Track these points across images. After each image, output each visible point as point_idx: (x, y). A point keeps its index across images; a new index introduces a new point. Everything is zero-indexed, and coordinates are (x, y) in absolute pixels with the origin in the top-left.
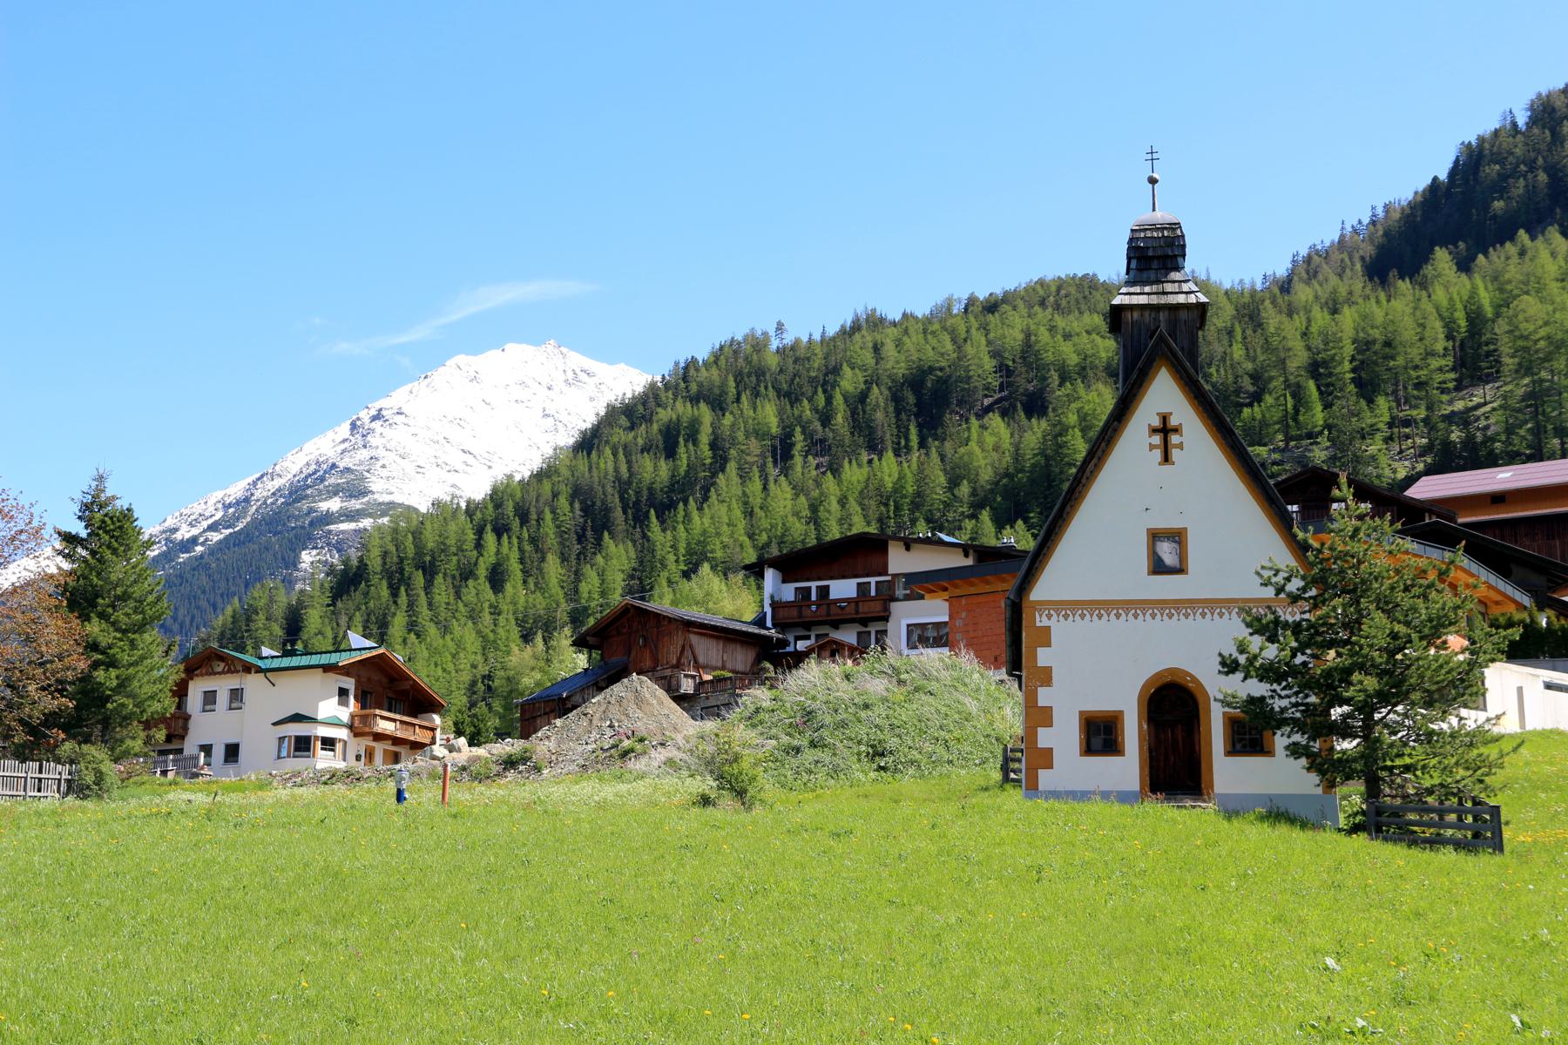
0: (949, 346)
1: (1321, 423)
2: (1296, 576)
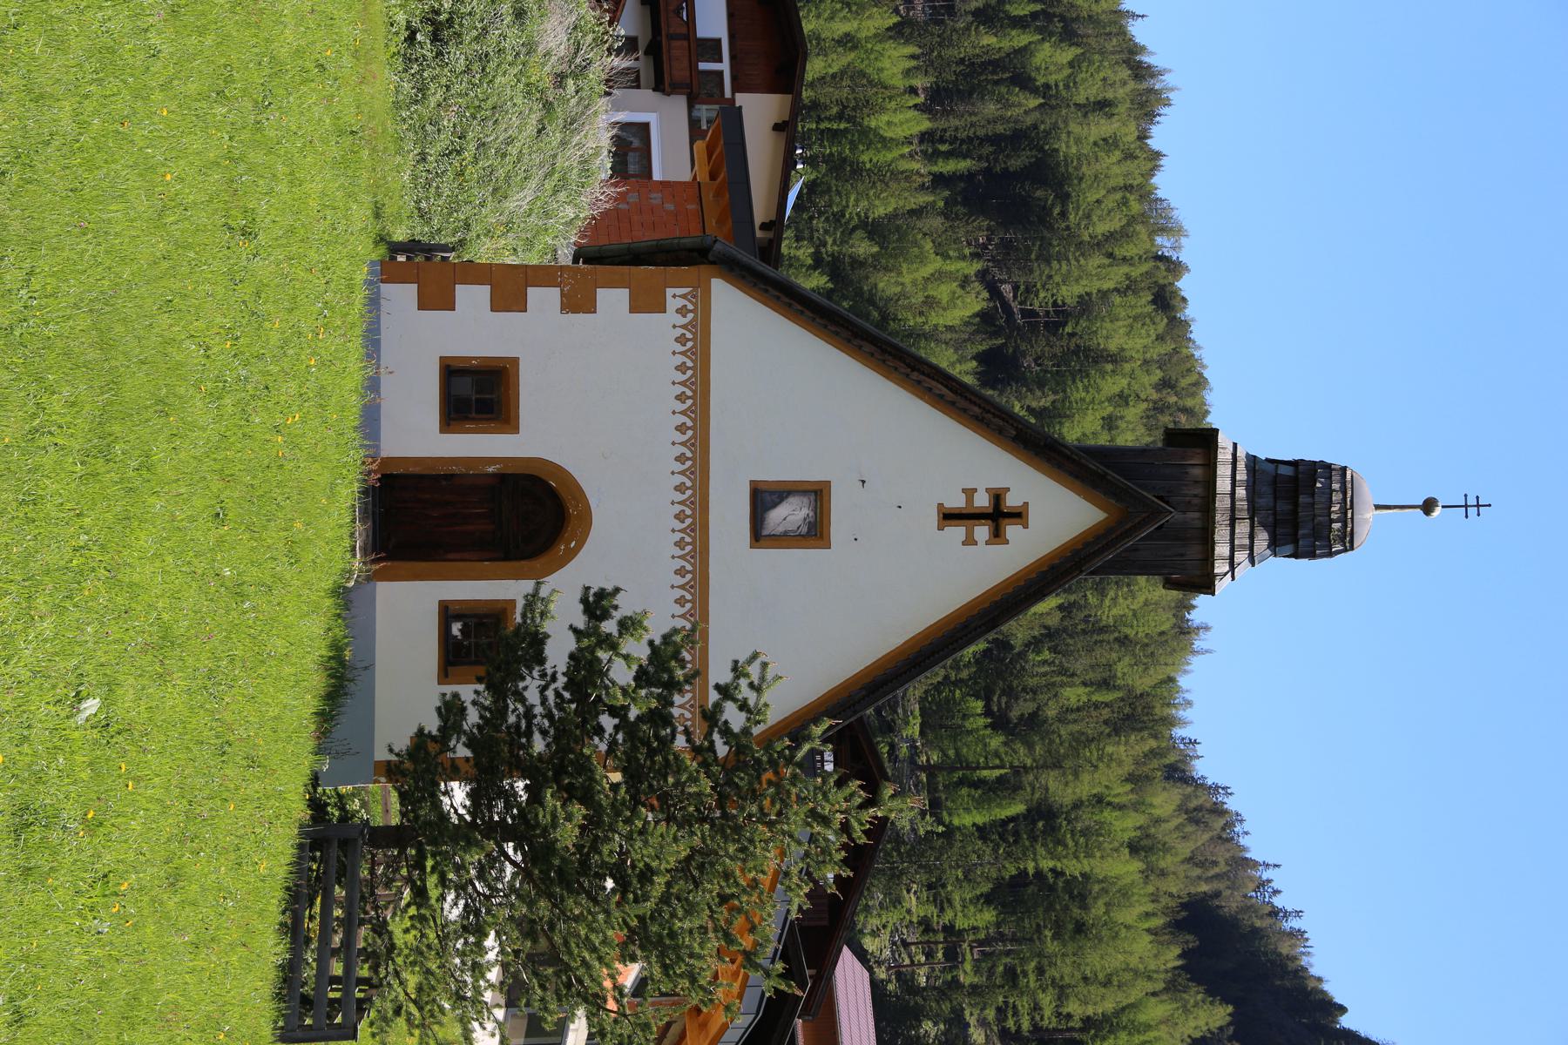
0: (1101, 228)
1: (956, 822)
2: (748, 719)
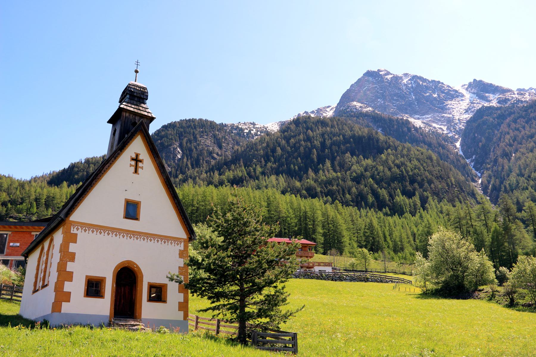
1: (35, 212)
